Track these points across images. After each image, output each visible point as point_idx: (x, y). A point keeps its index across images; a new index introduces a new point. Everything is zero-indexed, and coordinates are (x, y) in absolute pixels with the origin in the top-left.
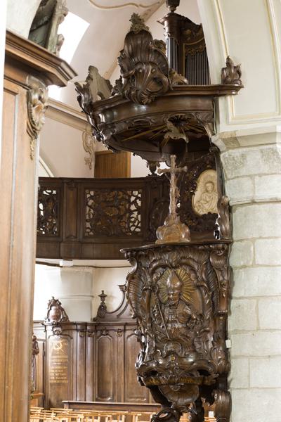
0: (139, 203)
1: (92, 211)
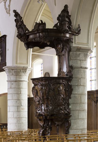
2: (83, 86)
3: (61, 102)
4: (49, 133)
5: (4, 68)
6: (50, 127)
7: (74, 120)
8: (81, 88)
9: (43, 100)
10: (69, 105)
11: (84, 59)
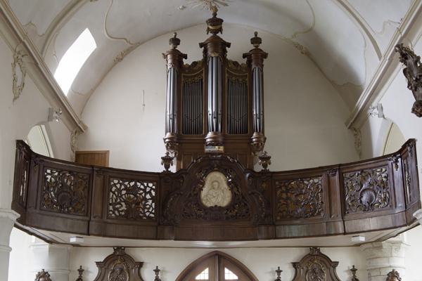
0: (153, 193)
1: (114, 197)
5: (417, 215)
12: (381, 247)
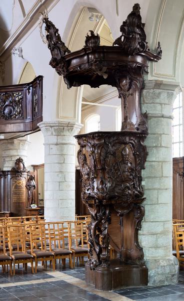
2: (165, 147)
3: (127, 175)
4: (105, 228)
5: (40, 125)
6: (107, 218)
7: (149, 206)
8: (162, 151)
9: (96, 172)
10: (140, 179)
11: (167, 102)
12: (12, 143)
